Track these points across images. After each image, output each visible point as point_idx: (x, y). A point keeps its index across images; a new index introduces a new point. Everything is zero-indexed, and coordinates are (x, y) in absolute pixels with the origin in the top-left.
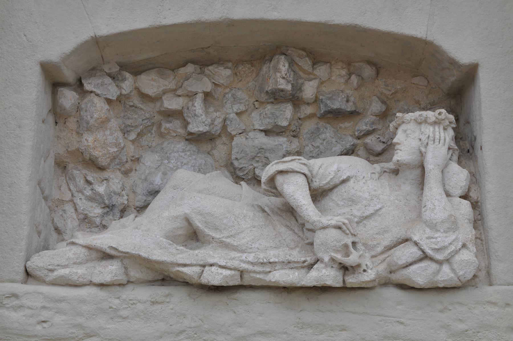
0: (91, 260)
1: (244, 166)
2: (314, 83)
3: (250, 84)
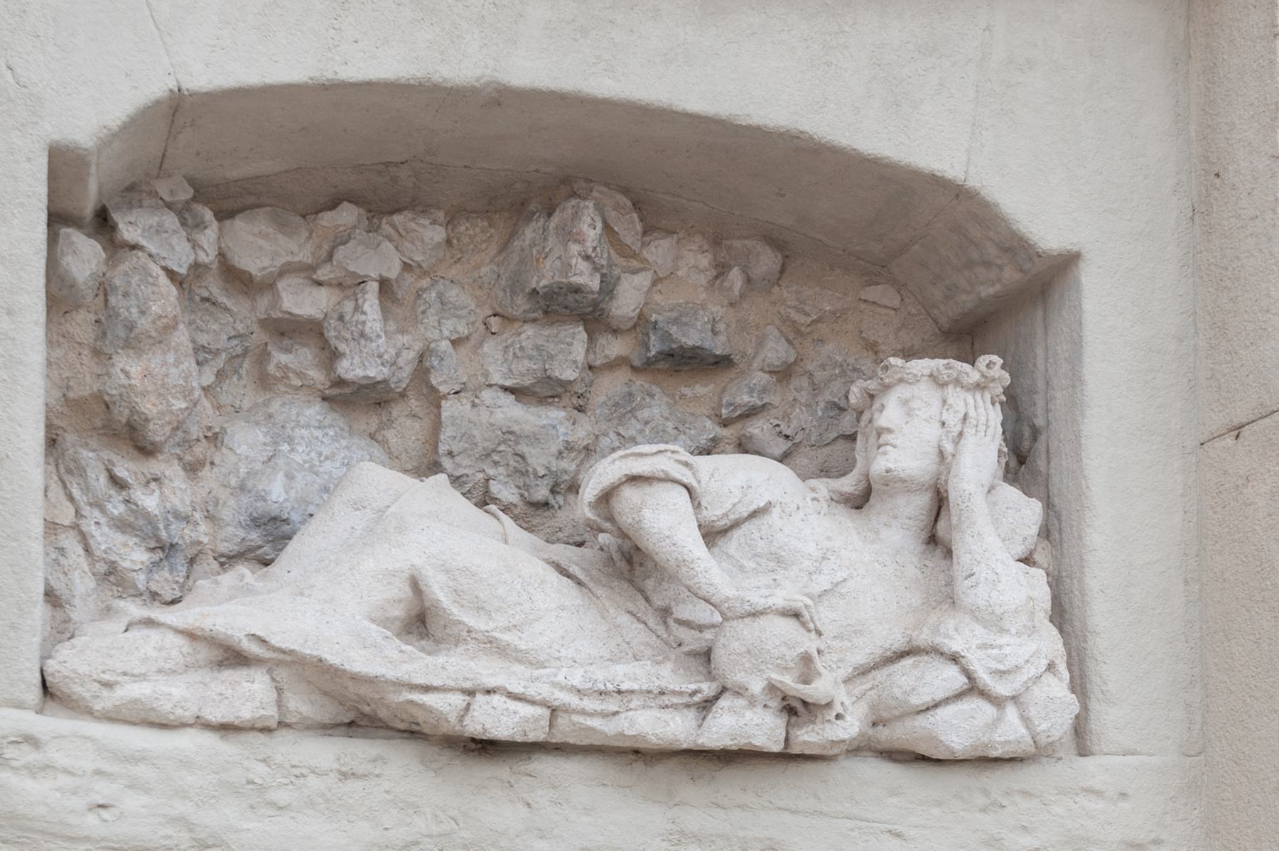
0: (196, 666)
1: (466, 471)
2: (643, 280)
3: (484, 270)
